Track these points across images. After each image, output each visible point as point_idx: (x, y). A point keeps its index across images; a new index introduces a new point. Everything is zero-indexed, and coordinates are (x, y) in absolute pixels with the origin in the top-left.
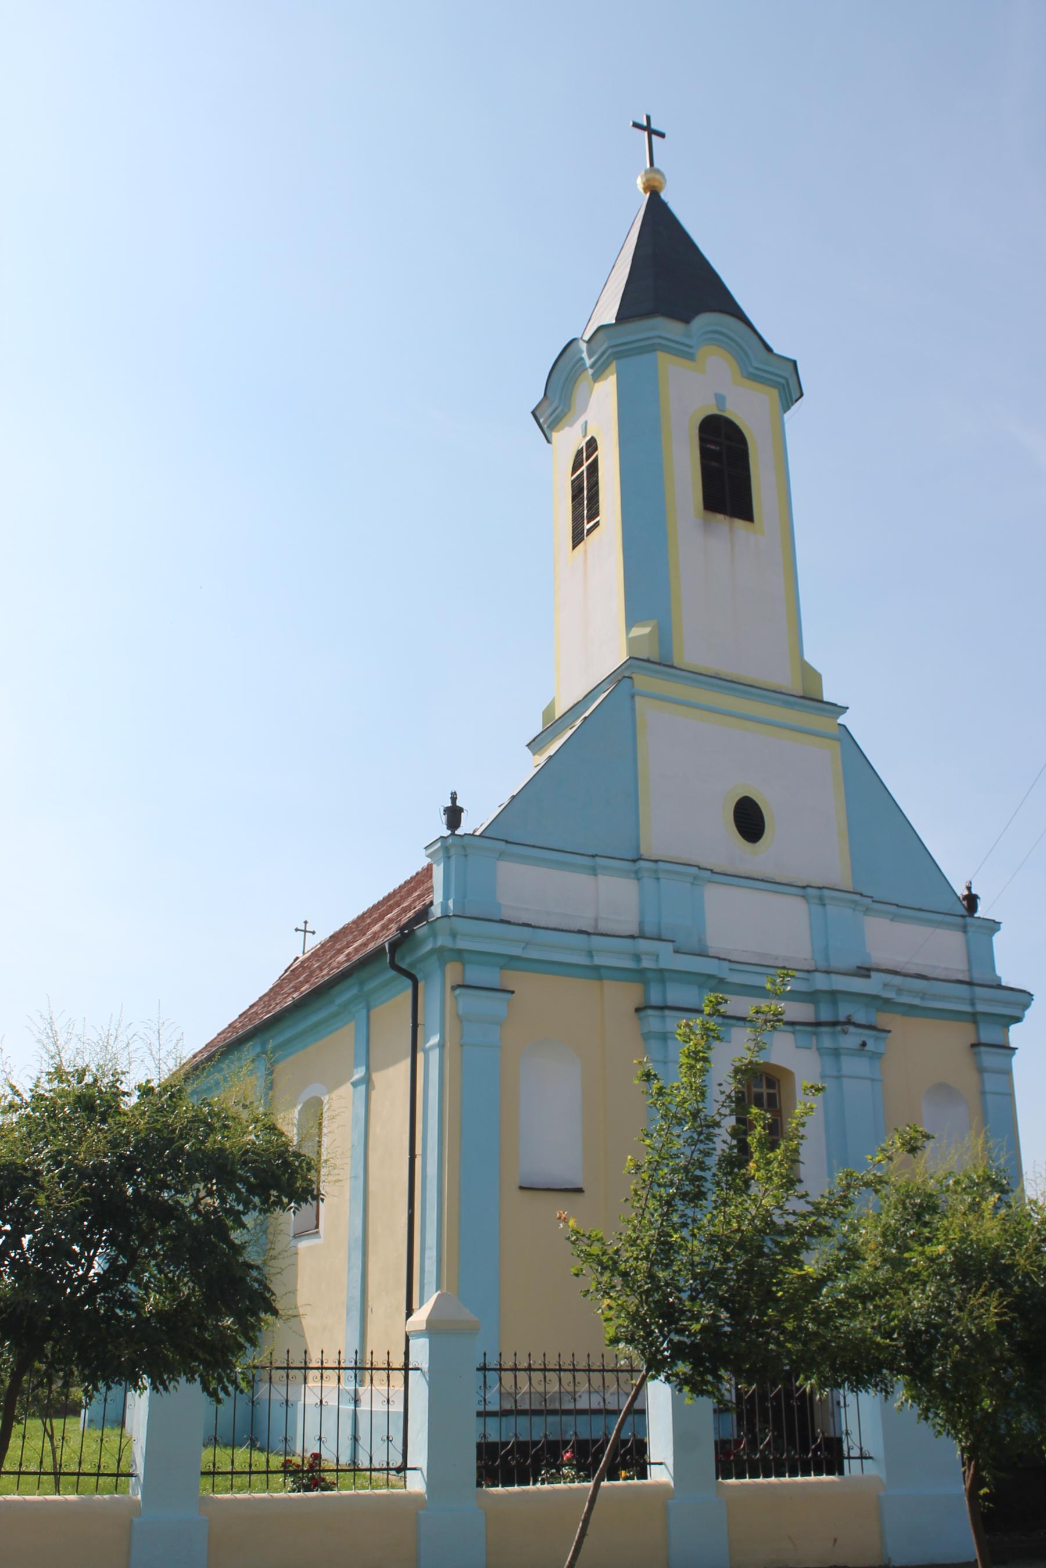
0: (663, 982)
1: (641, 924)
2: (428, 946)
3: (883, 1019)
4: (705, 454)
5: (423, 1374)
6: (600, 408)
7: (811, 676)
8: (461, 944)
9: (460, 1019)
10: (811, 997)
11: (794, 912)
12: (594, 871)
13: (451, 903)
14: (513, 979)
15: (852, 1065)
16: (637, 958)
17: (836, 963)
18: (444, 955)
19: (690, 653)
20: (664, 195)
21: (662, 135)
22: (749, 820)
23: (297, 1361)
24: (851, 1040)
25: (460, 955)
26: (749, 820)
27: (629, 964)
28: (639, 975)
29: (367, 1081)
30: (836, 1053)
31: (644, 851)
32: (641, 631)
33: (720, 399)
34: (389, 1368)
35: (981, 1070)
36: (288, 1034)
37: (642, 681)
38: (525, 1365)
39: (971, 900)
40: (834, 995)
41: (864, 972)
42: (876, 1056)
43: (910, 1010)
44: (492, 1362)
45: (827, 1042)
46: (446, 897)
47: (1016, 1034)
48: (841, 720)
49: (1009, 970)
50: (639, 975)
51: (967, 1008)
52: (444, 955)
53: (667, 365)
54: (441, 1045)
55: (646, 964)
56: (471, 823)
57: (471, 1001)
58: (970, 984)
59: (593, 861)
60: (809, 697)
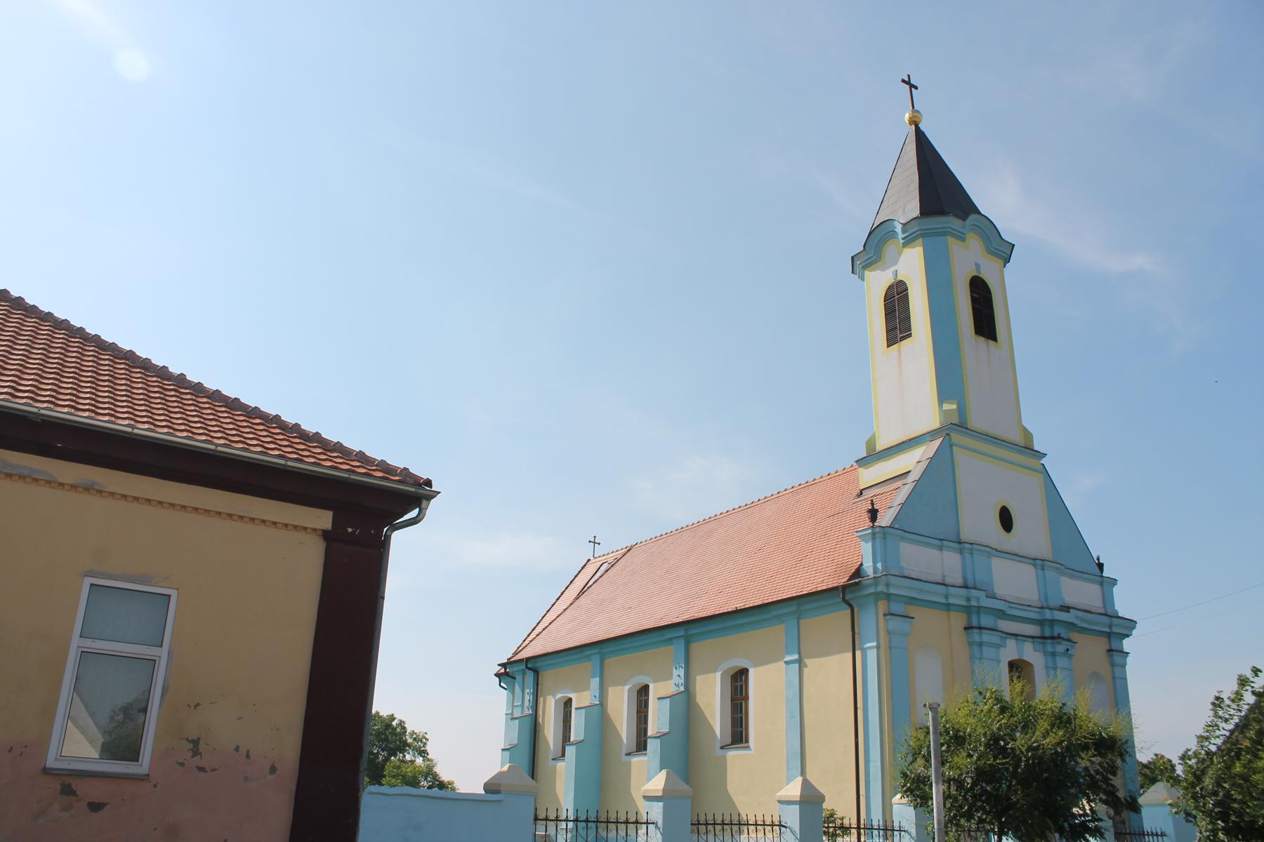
0: (978, 613)
1: (965, 579)
2: (872, 590)
3: (1075, 636)
4: (974, 300)
5: (657, 827)
6: (910, 265)
7: (1028, 435)
8: (892, 591)
9: (888, 632)
10: (1041, 623)
11: (1028, 572)
12: (941, 548)
13: (879, 565)
14: (913, 610)
15: (1061, 662)
16: (968, 599)
17: (1053, 603)
18: (877, 596)
19: (975, 422)
20: (922, 126)
21: (903, 81)
22: (1006, 520)
23: (613, 818)
24: (1060, 648)
25: (888, 597)
26: (1006, 520)
27: (964, 603)
28: (968, 610)
29: (800, 661)
30: (1053, 654)
31: (964, 537)
32: (946, 407)
33: (977, 266)
34: (608, 822)
35: (1113, 665)
36: (706, 629)
37: (956, 438)
38: (634, 819)
39: (1100, 566)
40: (1052, 622)
41: (1066, 609)
42: (1070, 656)
43: (1083, 630)
44: (702, 820)
45: (1049, 649)
46: (875, 562)
47: (1127, 644)
48: (1042, 461)
49: (1124, 606)
50: (968, 610)
51: (943, 601)
52: (877, 596)
53: (952, 243)
54: (878, 647)
55: (974, 603)
56: (885, 519)
57: (895, 623)
58: (966, 587)
59: (940, 542)
60: (1028, 449)
